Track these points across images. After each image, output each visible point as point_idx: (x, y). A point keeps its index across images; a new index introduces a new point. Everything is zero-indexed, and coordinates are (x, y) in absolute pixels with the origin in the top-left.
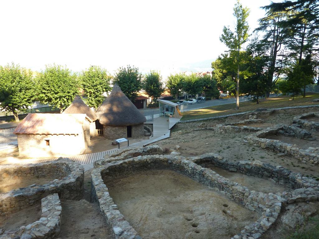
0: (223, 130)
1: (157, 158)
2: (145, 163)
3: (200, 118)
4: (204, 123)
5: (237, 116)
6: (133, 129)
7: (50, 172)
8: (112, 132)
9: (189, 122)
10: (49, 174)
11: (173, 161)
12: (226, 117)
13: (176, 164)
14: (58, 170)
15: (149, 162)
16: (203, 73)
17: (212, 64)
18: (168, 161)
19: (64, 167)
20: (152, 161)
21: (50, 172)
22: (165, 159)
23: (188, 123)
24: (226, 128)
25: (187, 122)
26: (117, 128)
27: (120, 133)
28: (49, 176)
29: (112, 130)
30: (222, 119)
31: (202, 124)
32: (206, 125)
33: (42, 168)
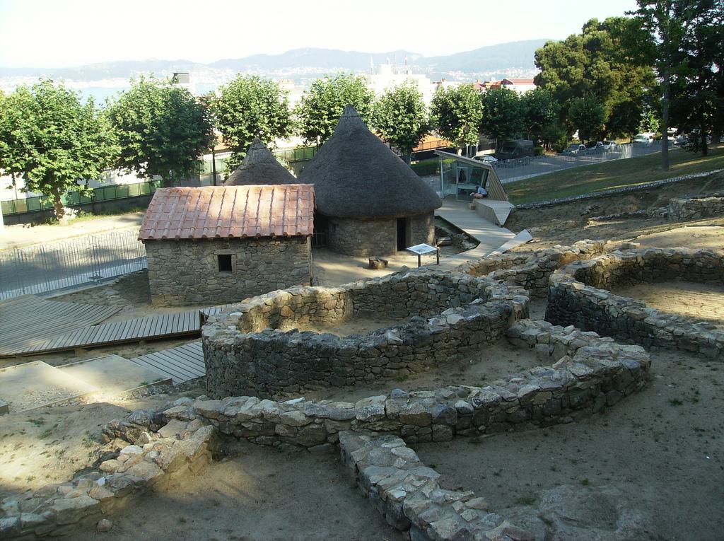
0: (696, 209)
1: (659, 255)
2: (634, 267)
3: (578, 194)
4: (597, 204)
5: (687, 181)
6: (412, 225)
7: (385, 302)
8: (359, 236)
9: (549, 206)
10: (381, 309)
11: (695, 261)
12: (659, 187)
13: (704, 267)
14: (410, 297)
15: (642, 264)
16: (492, 83)
17: (536, 55)
18: (682, 261)
19: (432, 286)
20: (647, 261)
21: (385, 302)
22: (675, 257)
23: (547, 209)
24: (704, 205)
25: (543, 206)
26: (371, 225)
27: (378, 238)
28: (382, 313)
29: (357, 232)
30: (647, 192)
31: (589, 207)
32: (601, 210)
33: (366, 295)
